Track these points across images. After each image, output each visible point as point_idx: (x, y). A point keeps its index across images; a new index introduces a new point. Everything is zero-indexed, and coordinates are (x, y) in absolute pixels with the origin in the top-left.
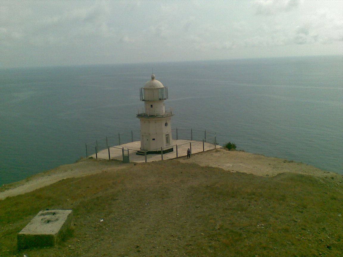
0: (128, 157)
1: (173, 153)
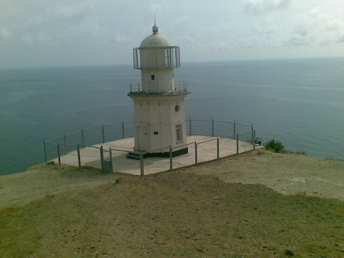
0: (111, 163)
1: (188, 156)
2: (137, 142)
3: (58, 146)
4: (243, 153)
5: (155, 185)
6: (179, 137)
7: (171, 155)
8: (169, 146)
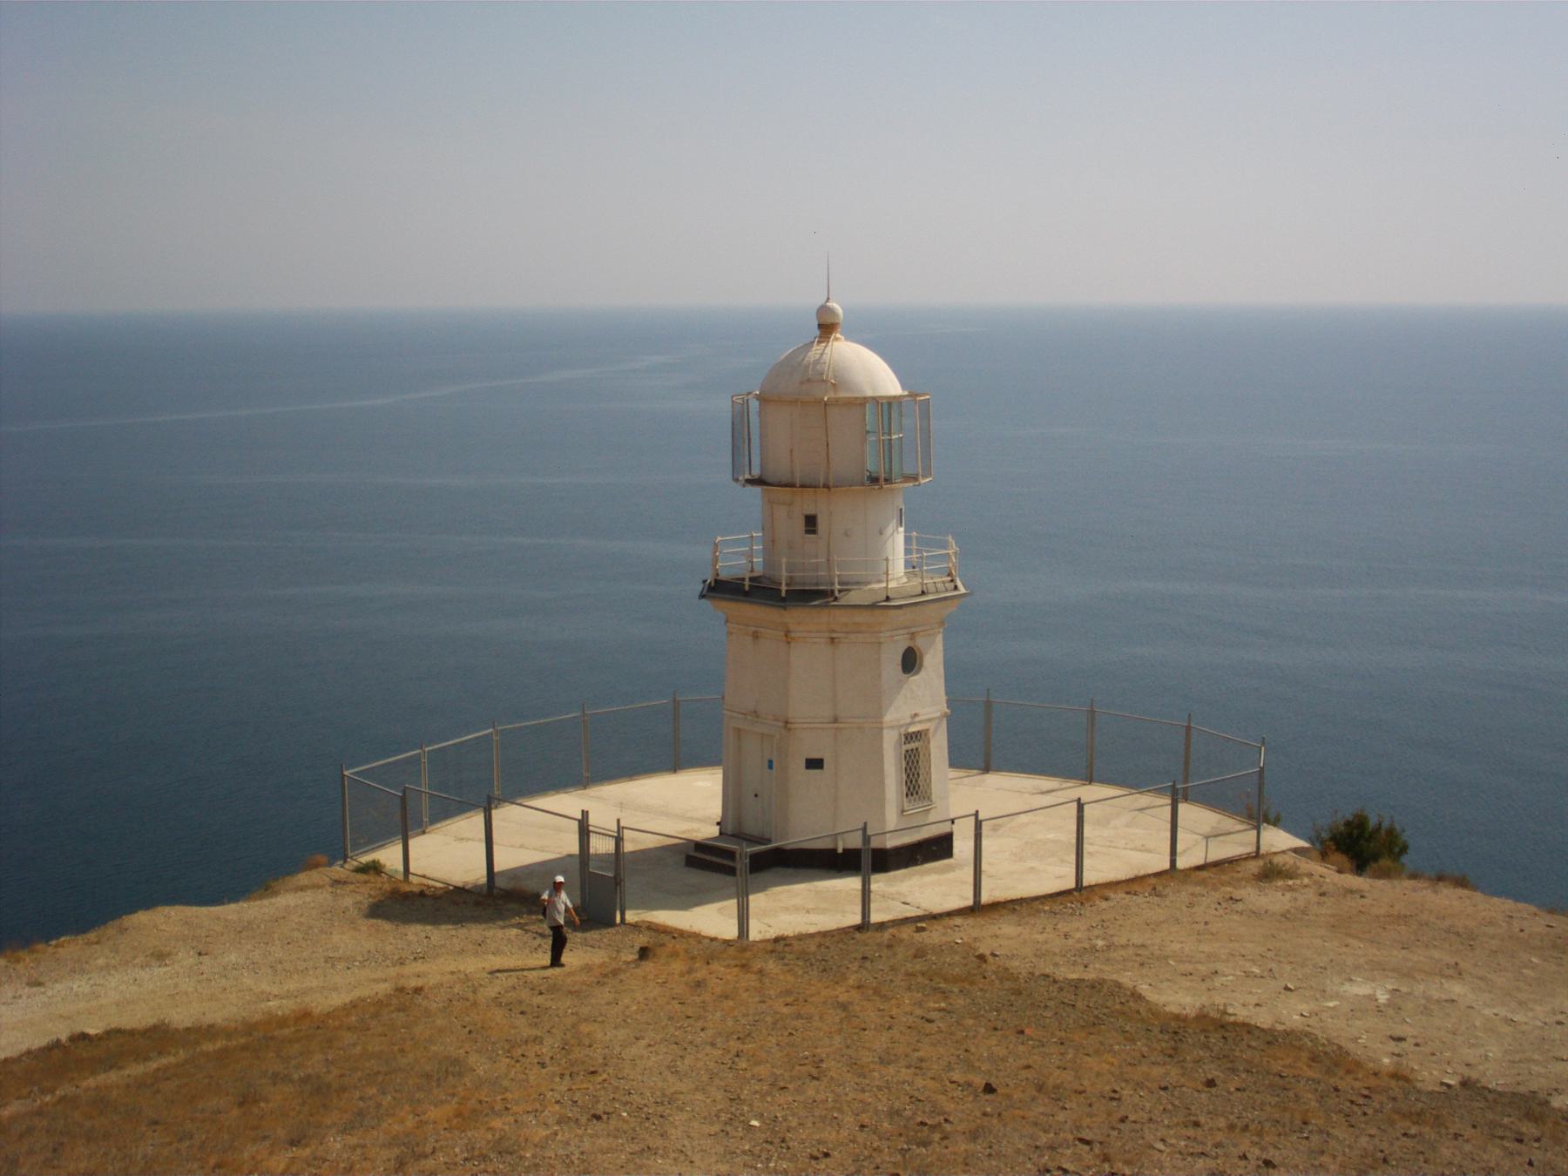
1: (951, 868)
2: (733, 794)
3: (403, 799)
4: (1199, 868)
5: (772, 966)
6: (915, 785)
7: (866, 860)
8: (861, 826)
